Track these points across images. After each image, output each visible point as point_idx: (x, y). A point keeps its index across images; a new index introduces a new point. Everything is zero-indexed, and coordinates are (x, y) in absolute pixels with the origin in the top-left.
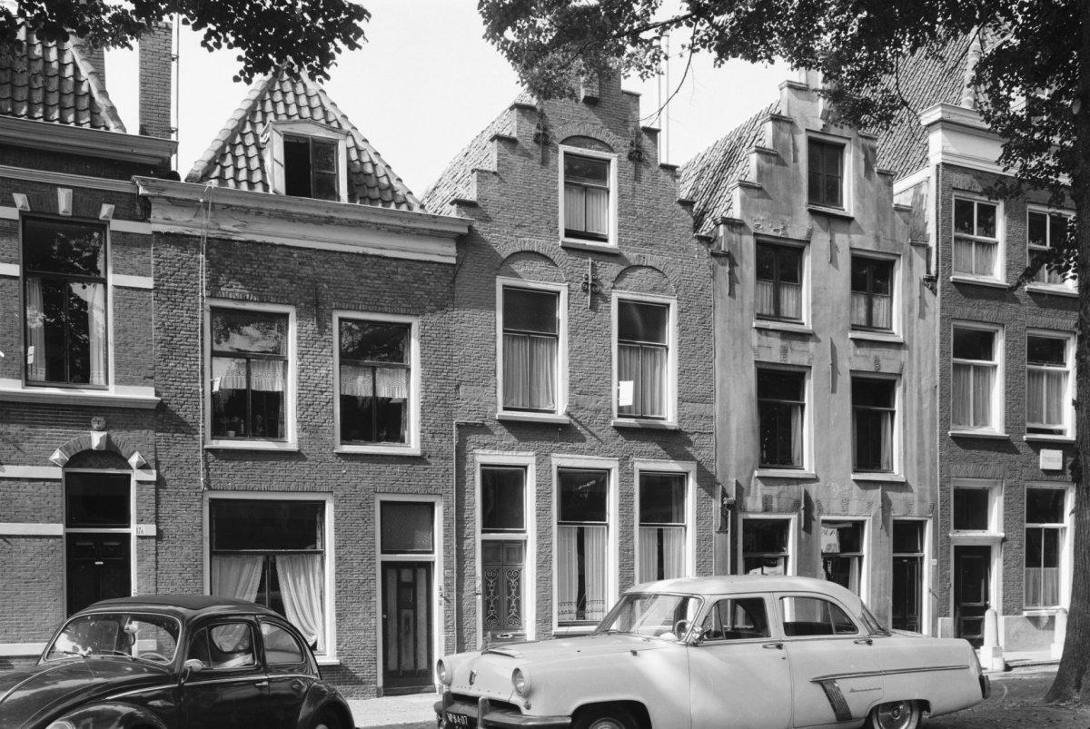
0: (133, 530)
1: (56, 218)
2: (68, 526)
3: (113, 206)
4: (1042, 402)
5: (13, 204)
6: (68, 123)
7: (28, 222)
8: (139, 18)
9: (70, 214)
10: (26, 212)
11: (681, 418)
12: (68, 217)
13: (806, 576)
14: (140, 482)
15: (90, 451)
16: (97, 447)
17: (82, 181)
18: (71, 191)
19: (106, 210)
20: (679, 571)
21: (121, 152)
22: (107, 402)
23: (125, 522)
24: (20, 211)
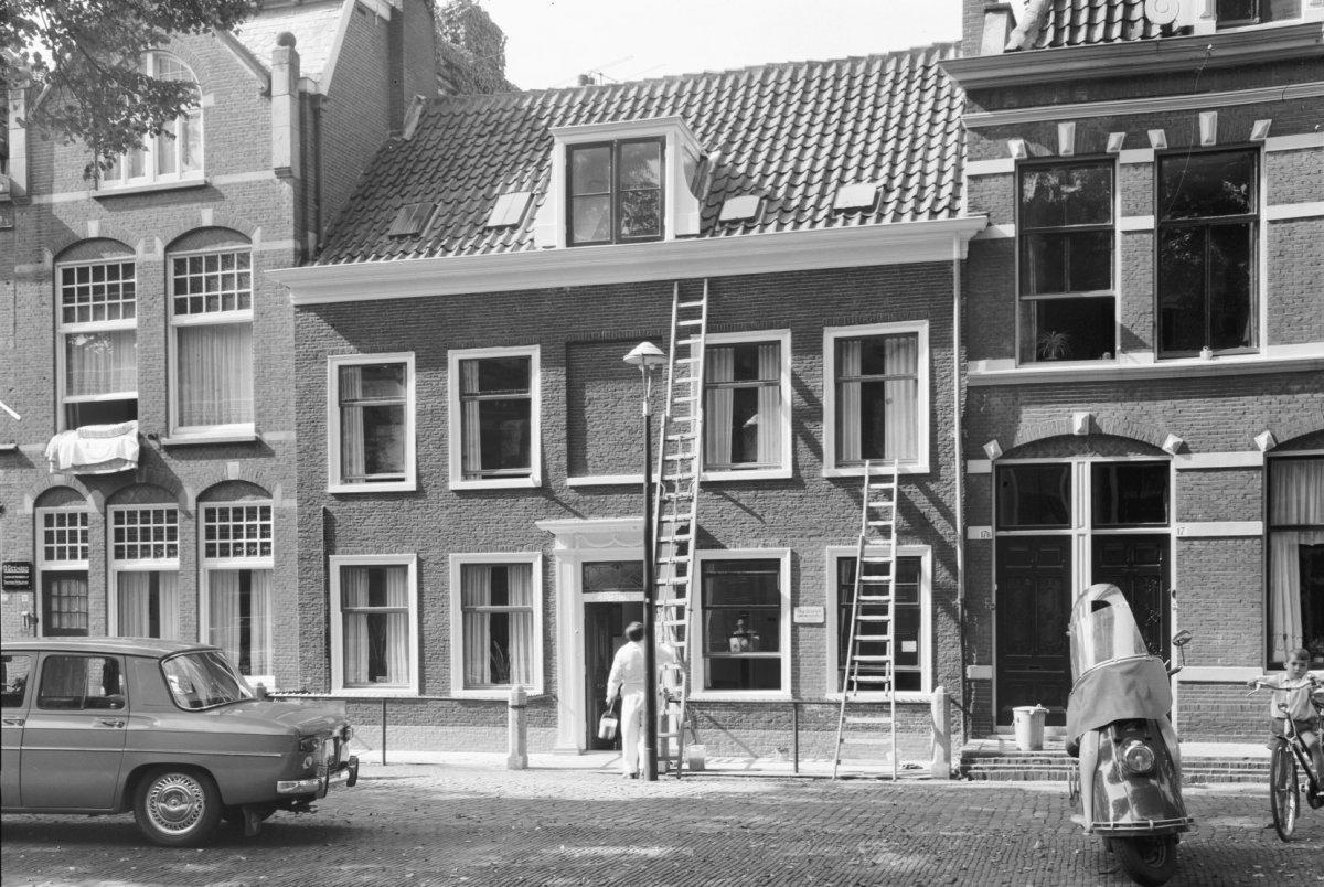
0: (1175, 529)
1: (1201, 150)
2: (998, 529)
3: (1123, 134)
4: (1021, 332)
5: (1148, 145)
6: (1113, 40)
7: (1166, 163)
8: (57, 20)
9: (1166, 147)
10: (1023, 161)
11: (248, 421)
12: (1071, 157)
13: (886, 628)
14: (1181, 471)
15: (1073, 435)
16: (1079, 431)
17: (1138, 106)
18: (1215, 113)
19: (1114, 140)
20: (128, 630)
21: (1132, 65)
22: (1244, 368)
23: (1160, 516)
24: (1156, 152)
